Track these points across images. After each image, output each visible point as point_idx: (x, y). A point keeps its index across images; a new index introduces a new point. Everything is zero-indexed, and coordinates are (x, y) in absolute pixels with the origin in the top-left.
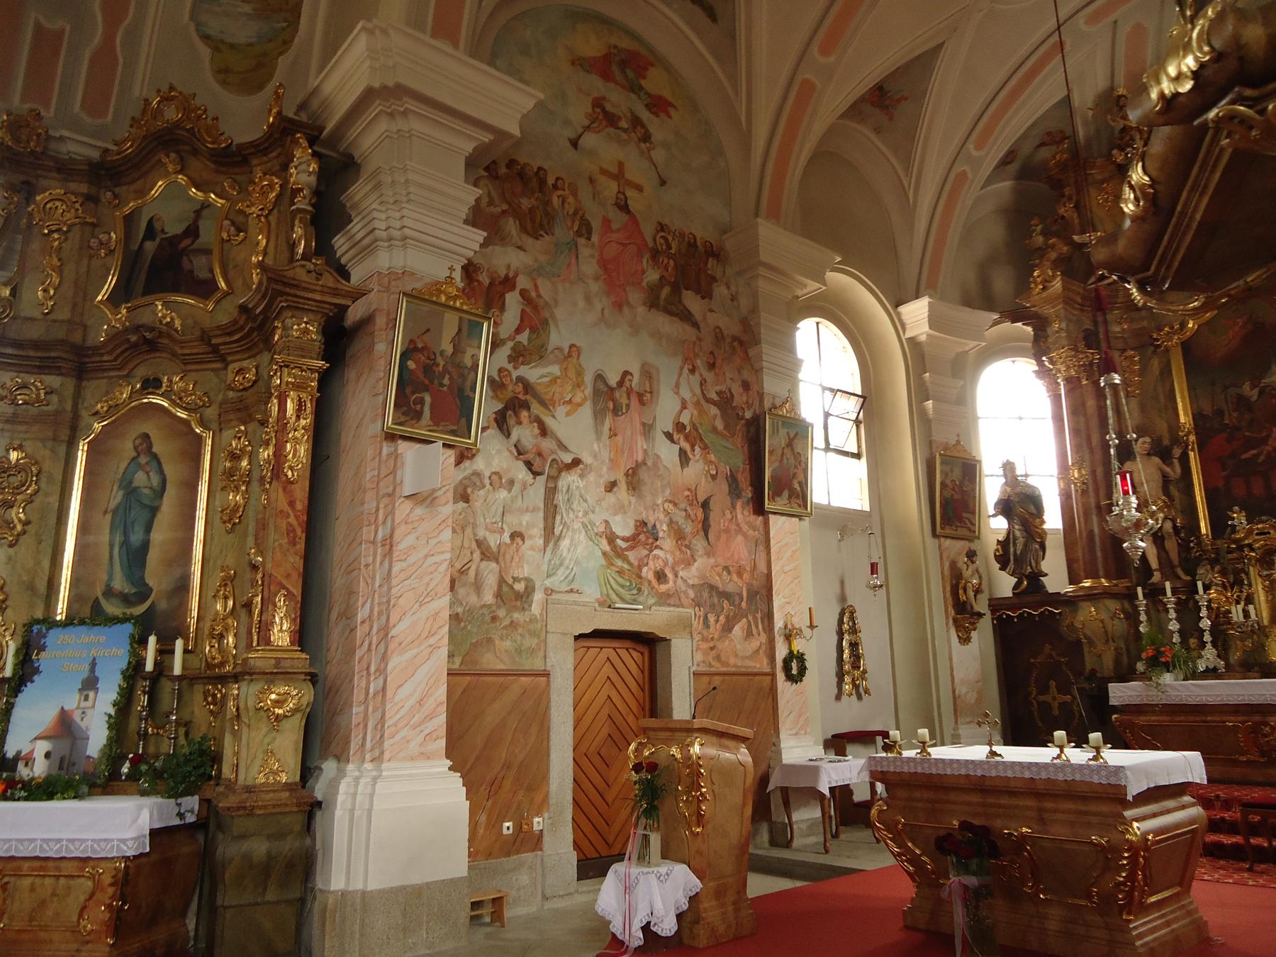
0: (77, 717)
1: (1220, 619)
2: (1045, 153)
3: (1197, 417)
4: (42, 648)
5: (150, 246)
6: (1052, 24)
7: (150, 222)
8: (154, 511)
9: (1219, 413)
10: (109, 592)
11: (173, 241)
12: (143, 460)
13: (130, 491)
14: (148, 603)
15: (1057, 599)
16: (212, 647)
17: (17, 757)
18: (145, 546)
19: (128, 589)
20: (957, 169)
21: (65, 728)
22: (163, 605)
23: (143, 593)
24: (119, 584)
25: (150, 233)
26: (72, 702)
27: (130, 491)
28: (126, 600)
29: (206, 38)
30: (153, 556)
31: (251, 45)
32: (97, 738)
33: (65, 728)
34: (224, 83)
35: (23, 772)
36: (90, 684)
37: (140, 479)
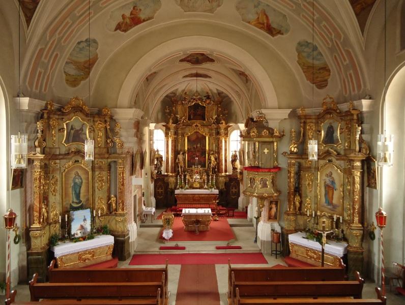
0: (84, 225)
1: (189, 180)
2: (170, 95)
3: (188, 149)
4: (74, 215)
5: (72, 132)
6: (91, 21)
7: (72, 126)
8: (80, 187)
9: (191, 149)
10: (73, 202)
11: (77, 131)
12: (77, 177)
13: (75, 183)
14: (81, 204)
15: (164, 175)
16: (311, 257)
17: (74, 234)
18: (80, 193)
19: (77, 201)
20: (55, 53)
21: (82, 227)
22: (84, 203)
23: (80, 202)
24: (75, 200)
25: (72, 128)
26: (82, 223)
27: (75, 183)
28: (77, 203)
29: (65, 72)
30: (82, 195)
31: (73, 75)
32: (89, 228)
33: (82, 227)
34: (67, 83)
35: (76, 236)
36: (85, 220)
37: (77, 180)
